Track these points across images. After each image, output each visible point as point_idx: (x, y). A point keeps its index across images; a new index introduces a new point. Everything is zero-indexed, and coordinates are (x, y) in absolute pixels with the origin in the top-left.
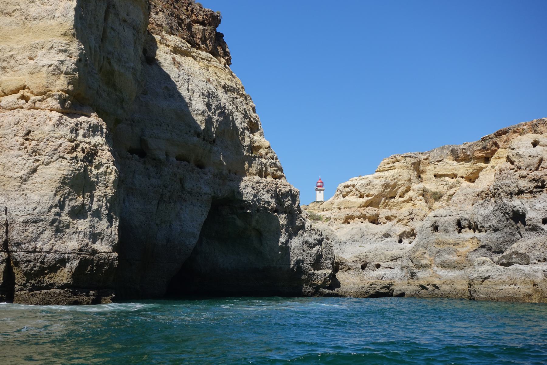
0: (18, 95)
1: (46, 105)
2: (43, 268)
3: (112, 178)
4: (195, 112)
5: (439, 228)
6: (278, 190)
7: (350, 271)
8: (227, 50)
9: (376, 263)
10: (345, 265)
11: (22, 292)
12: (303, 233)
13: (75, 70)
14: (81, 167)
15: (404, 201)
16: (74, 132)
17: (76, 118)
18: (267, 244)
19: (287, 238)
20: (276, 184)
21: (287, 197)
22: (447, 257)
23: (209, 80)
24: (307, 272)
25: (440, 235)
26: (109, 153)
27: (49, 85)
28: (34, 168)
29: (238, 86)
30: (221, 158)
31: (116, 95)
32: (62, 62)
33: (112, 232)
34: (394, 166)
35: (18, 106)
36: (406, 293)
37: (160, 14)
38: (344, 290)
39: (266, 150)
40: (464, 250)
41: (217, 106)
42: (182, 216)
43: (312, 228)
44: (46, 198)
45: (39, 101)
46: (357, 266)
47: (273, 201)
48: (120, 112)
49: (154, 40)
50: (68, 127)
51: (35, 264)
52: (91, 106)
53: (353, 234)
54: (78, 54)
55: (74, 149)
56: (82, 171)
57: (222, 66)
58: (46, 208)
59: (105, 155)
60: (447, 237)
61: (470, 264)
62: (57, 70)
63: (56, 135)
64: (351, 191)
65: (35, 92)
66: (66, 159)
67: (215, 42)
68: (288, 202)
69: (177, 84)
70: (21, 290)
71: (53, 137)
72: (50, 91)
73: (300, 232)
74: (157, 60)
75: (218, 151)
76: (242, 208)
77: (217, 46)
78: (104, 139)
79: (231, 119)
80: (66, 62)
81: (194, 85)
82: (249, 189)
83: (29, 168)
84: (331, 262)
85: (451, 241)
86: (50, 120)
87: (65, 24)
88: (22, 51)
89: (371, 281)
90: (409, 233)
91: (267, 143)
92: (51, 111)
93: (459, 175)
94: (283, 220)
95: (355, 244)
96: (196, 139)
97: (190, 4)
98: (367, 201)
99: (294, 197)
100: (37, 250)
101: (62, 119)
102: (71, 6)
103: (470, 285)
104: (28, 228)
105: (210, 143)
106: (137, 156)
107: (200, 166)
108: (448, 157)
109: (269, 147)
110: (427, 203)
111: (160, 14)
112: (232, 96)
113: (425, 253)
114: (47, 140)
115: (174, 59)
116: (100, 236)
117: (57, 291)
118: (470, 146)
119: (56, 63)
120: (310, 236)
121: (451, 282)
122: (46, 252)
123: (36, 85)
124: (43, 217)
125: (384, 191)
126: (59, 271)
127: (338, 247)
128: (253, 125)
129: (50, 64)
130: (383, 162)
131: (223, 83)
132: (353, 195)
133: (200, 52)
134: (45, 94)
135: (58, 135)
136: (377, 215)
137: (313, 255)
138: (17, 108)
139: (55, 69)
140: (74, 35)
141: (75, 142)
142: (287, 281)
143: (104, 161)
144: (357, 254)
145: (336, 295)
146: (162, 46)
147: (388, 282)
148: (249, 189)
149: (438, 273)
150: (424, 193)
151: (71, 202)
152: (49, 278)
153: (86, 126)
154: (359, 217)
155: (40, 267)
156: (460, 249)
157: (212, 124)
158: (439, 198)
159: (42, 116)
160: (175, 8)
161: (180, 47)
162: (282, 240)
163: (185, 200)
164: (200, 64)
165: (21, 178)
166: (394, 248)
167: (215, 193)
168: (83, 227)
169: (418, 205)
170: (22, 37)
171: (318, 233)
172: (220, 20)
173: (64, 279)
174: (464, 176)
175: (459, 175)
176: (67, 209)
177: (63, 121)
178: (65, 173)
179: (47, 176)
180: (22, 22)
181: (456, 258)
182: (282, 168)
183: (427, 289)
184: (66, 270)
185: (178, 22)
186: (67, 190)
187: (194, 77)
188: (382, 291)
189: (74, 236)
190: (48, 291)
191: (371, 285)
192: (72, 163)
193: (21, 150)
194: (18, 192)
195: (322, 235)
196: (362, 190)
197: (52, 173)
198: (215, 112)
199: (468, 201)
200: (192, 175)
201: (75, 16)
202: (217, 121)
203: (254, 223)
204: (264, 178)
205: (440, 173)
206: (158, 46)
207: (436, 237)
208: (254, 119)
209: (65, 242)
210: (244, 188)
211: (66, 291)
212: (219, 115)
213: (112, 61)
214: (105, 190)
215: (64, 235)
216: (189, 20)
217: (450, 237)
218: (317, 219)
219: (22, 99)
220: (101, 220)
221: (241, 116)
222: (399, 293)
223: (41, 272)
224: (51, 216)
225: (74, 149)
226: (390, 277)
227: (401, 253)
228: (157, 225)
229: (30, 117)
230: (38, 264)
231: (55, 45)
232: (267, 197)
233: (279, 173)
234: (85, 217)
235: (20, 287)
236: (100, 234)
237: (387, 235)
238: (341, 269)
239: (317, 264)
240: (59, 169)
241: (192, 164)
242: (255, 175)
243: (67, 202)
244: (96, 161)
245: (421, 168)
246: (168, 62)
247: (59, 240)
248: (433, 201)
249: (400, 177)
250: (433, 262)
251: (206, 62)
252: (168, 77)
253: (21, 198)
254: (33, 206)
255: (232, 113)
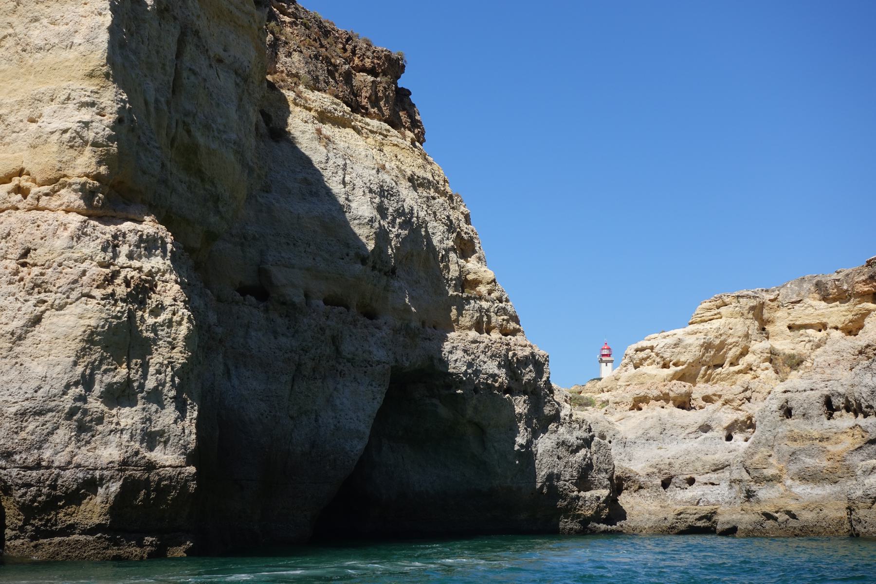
0: (10, 186)
1: (59, 203)
2: (55, 496)
3: (182, 332)
4: (357, 222)
5: (793, 412)
6: (511, 354)
7: (642, 491)
8: (418, 117)
9: (688, 476)
10: (634, 482)
11: (18, 542)
12: (557, 427)
13: (110, 138)
14: (123, 313)
15: (739, 372)
16: (110, 250)
17: (116, 224)
18: (494, 447)
19: (530, 436)
20: (508, 344)
21: (526, 365)
22: (810, 462)
23: (384, 168)
24: (567, 495)
25: (795, 424)
26: (177, 287)
27: (63, 166)
28: (36, 316)
29: (436, 178)
30: (407, 300)
31: (205, 189)
32: (86, 125)
33: (184, 429)
34: (719, 313)
35: (9, 205)
36: (739, 527)
37: (296, 56)
38: (632, 525)
39: (489, 287)
40: (839, 448)
41: (397, 211)
42: (338, 402)
43: (573, 418)
44: (58, 369)
45: (47, 195)
46: (655, 482)
47: (502, 373)
48: (213, 219)
49: (284, 99)
50: (99, 241)
51: (39, 490)
52: (143, 202)
53: (647, 427)
54: (115, 109)
55: (110, 280)
56: (124, 319)
57: (409, 143)
58: (58, 387)
59: (170, 291)
60: (808, 428)
61: (850, 472)
62: (77, 139)
63: (75, 256)
64: (648, 357)
65: (38, 179)
66: (93, 297)
67: (395, 104)
68: (528, 375)
69: (324, 173)
70: (16, 537)
71: (69, 259)
72: (65, 176)
73: (552, 426)
74: (289, 133)
75: (400, 288)
76: (449, 387)
77: (400, 110)
78: (168, 262)
79: (423, 233)
80: (94, 124)
81: (354, 175)
82: (459, 354)
83: (27, 317)
84: (607, 476)
85: (816, 434)
86: (65, 229)
87: (92, 56)
88: (17, 107)
89: (680, 508)
90: (744, 422)
91: (490, 275)
92: (67, 212)
93: (830, 325)
94: (520, 406)
95: (650, 444)
96: (359, 267)
97: (349, 39)
98: (676, 372)
99: (539, 365)
100: (44, 464)
101: (86, 227)
102: (103, 25)
103: (850, 509)
104: (25, 424)
105: (385, 274)
106: (253, 299)
107: (371, 315)
108: (811, 295)
109: (494, 281)
110: (777, 373)
111: (296, 56)
112: (425, 194)
113: (770, 456)
114: (60, 265)
115: (319, 131)
116: (161, 436)
117: (82, 538)
118: (847, 275)
119: (75, 126)
120: (570, 432)
121: (818, 506)
122: (59, 467)
123: (41, 167)
124: (53, 404)
125: (703, 355)
126: (85, 501)
127: (621, 450)
128: (465, 244)
129: (65, 128)
130: (700, 306)
131: (409, 173)
132: (651, 364)
133: (368, 120)
134: (56, 182)
135: (80, 255)
136: (689, 395)
137: (576, 465)
138: (7, 209)
139: (74, 138)
140: (107, 76)
141: (112, 267)
142: (532, 512)
143: (168, 301)
144: (654, 462)
145: (618, 533)
146: (298, 109)
147: (709, 508)
148: (459, 354)
149: (793, 490)
150: (772, 357)
151: (105, 376)
152: (66, 514)
153: (132, 238)
154: (657, 399)
155: (48, 495)
156: (831, 448)
157: (389, 241)
158: (798, 365)
159: (50, 222)
160: (322, 46)
161: (330, 112)
162: (520, 440)
163: (342, 374)
164: (368, 140)
165: (13, 334)
166: (718, 449)
167: (396, 361)
168: (130, 422)
169: (762, 376)
170: (18, 83)
171: (584, 427)
172: (403, 66)
173: (95, 516)
174: (840, 326)
175: (830, 325)
176: (98, 389)
177: (89, 230)
178: (93, 323)
179: (60, 330)
180: (18, 57)
181: (826, 464)
182: (516, 317)
183: (776, 519)
184: (98, 499)
185: (328, 70)
186: (97, 355)
187: (357, 164)
188: (700, 524)
189: (111, 437)
190: (66, 538)
191: (679, 514)
192: (104, 306)
193: (13, 283)
194: (7, 360)
195: (590, 430)
196: (667, 355)
197: (68, 323)
198: (393, 222)
199: (843, 363)
200: (354, 331)
201: (109, 42)
202: (398, 236)
203: (470, 412)
204: (485, 335)
205: (798, 323)
206: (291, 109)
207: (789, 428)
208: (466, 233)
209: (95, 448)
210: (451, 352)
211: (99, 538)
212: (401, 226)
213: (193, 129)
214: (169, 354)
215: (93, 436)
216: (347, 67)
217: (814, 428)
218: (587, 405)
219: (16, 194)
220: (163, 407)
221: (442, 228)
222: (727, 527)
223: (52, 504)
224: (68, 402)
225: (110, 280)
226: (712, 500)
227: (731, 457)
228: (292, 418)
229: (28, 224)
230: (45, 490)
231: (73, 95)
232: (491, 367)
233: (512, 325)
234: (132, 403)
235: (14, 532)
236: (161, 433)
237: (705, 428)
238: (626, 489)
239: (584, 480)
240: (80, 317)
241: (354, 310)
242: (470, 329)
243: (98, 377)
244: (152, 302)
245: (766, 314)
246: (308, 136)
247: (85, 445)
248: (788, 369)
249: (731, 331)
250: (785, 471)
251: (379, 138)
252: (307, 161)
253: (13, 371)
254: (35, 384)
255: (425, 222)
